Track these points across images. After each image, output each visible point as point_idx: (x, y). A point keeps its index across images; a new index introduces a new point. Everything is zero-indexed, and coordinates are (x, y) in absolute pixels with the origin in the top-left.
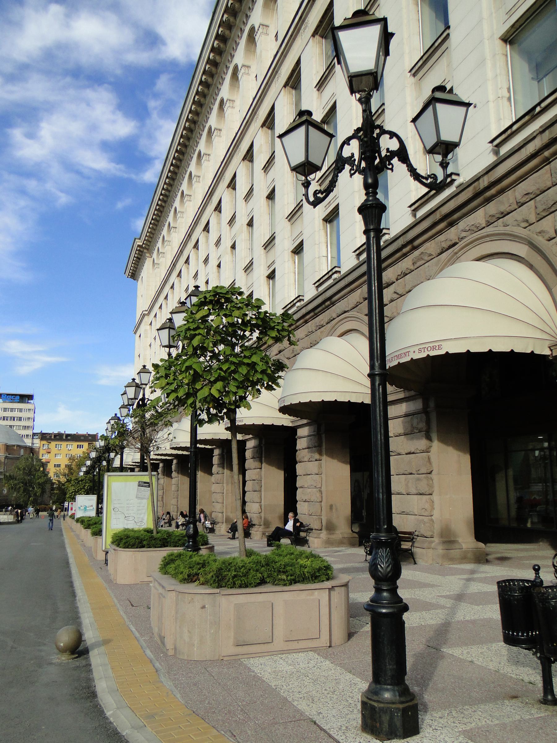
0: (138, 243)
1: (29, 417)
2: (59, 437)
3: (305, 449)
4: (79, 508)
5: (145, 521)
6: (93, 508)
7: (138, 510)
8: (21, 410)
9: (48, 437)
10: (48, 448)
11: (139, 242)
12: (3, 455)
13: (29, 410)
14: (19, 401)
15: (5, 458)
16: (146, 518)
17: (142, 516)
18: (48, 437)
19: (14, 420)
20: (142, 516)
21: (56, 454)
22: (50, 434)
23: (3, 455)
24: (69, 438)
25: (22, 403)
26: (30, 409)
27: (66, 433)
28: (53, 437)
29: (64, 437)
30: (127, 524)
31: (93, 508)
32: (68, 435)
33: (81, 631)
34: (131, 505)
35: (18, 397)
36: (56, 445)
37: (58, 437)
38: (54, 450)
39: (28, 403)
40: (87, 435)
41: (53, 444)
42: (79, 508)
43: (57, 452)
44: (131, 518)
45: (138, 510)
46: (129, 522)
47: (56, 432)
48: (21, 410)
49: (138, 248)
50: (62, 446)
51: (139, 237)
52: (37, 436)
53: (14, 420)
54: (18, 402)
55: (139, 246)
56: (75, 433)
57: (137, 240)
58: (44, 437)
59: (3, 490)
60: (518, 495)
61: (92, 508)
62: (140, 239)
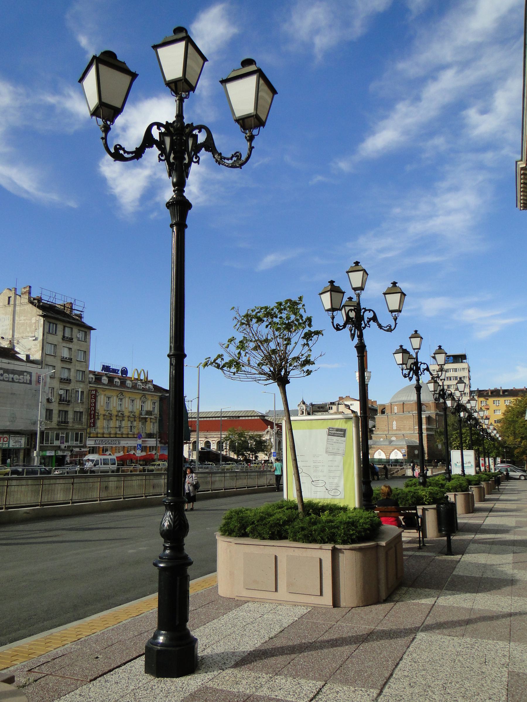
0: (521, 166)
1: (464, 375)
2: (496, 393)
3: (361, 349)
4: (456, 464)
5: (341, 489)
6: (472, 465)
7: (330, 471)
8: (456, 370)
9: (485, 394)
10: (487, 405)
11: (521, 164)
12: (434, 412)
13: (464, 369)
14: (452, 361)
15: (436, 415)
16: (342, 483)
17: (336, 481)
18: (485, 394)
19: (450, 380)
20: (336, 481)
21: (495, 410)
22: (486, 391)
23: (434, 412)
24: (506, 393)
25: (457, 362)
26: (464, 368)
27: (503, 388)
28: (490, 394)
29: (501, 393)
30: (316, 492)
31: (472, 465)
32: (505, 391)
33: (508, 589)
34: (319, 464)
35: (452, 358)
36: (494, 401)
37: (494, 394)
38: (492, 407)
39: (462, 362)
40: (525, 390)
41: (491, 400)
42: (456, 464)
43: (496, 408)
44: (321, 484)
45: (330, 471)
46: (319, 489)
47: (492, 389)
48: (456, 370)
49: (522, 172)
50: (500, 402)
51: (201, 61)
52: (474, 393)
53: (450, 380)
54: (453, 363)
55: (522, 169)
56: (512, 388)
57: (518, 163)
58: (481, 394)
59: (437, 446)
60: (378, 466)
61: (470, 465)
62: (521, 160)
